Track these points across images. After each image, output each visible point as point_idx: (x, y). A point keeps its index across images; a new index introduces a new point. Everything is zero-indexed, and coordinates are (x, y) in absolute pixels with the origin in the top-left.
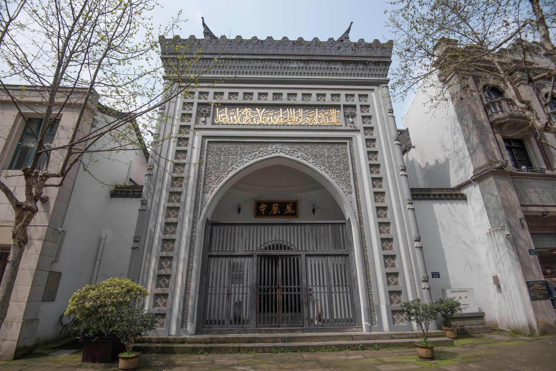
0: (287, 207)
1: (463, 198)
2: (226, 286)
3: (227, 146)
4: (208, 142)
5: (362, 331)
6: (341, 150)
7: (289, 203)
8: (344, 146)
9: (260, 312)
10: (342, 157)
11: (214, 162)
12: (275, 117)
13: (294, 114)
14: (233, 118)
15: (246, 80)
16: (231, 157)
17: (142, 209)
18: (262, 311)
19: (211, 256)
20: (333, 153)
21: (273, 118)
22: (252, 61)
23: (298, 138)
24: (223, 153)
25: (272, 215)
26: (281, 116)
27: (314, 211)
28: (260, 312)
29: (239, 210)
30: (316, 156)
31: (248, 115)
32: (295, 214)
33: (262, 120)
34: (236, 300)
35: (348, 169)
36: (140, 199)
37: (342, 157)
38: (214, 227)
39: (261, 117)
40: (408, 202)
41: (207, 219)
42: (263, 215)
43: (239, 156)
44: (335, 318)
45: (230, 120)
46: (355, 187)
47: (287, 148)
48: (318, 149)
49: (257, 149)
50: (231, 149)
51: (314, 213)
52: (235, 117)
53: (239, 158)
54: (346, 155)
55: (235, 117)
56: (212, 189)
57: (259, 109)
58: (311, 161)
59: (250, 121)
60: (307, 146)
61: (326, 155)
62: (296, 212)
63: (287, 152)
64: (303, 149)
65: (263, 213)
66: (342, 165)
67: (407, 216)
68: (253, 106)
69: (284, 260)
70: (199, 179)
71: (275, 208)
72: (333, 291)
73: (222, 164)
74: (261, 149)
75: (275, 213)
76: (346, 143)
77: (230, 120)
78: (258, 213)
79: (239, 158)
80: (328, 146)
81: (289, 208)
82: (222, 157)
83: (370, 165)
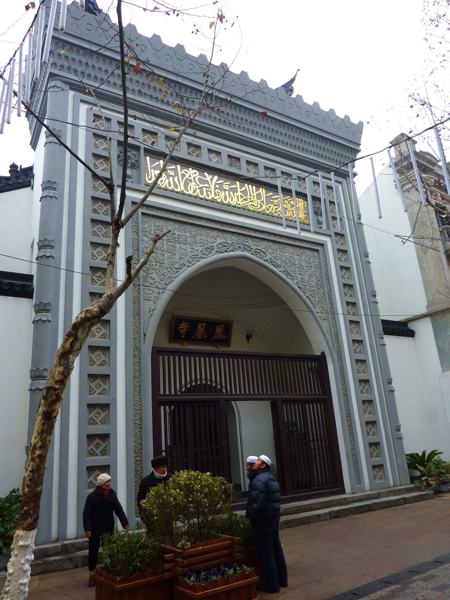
1: (411, 334)
5: (343, 492)
8: (315, 254)
12: (231, 193)
13: (255, 194)
14: (174, 181)
15: (216, 132)
16: (178, 246)
21: (230, 195)
22: (328, 142)
23: (281, 236)
25: (195, 340)
26: (239, 193)
31: (195, 182)
33: (216, 195)
39: (213, 188)
45: (169, 183)
51: (248, 341)
52: (176, 179)
53: (189, 250)
55: (176, 179)
57: (209, 174)
59: (198, 191)
65: (183, 337)
68: (202, 167)
69: (182, 409)
71: (201, 329)
76: (318, 251)
77: (169, 183)
81: (219, 330)
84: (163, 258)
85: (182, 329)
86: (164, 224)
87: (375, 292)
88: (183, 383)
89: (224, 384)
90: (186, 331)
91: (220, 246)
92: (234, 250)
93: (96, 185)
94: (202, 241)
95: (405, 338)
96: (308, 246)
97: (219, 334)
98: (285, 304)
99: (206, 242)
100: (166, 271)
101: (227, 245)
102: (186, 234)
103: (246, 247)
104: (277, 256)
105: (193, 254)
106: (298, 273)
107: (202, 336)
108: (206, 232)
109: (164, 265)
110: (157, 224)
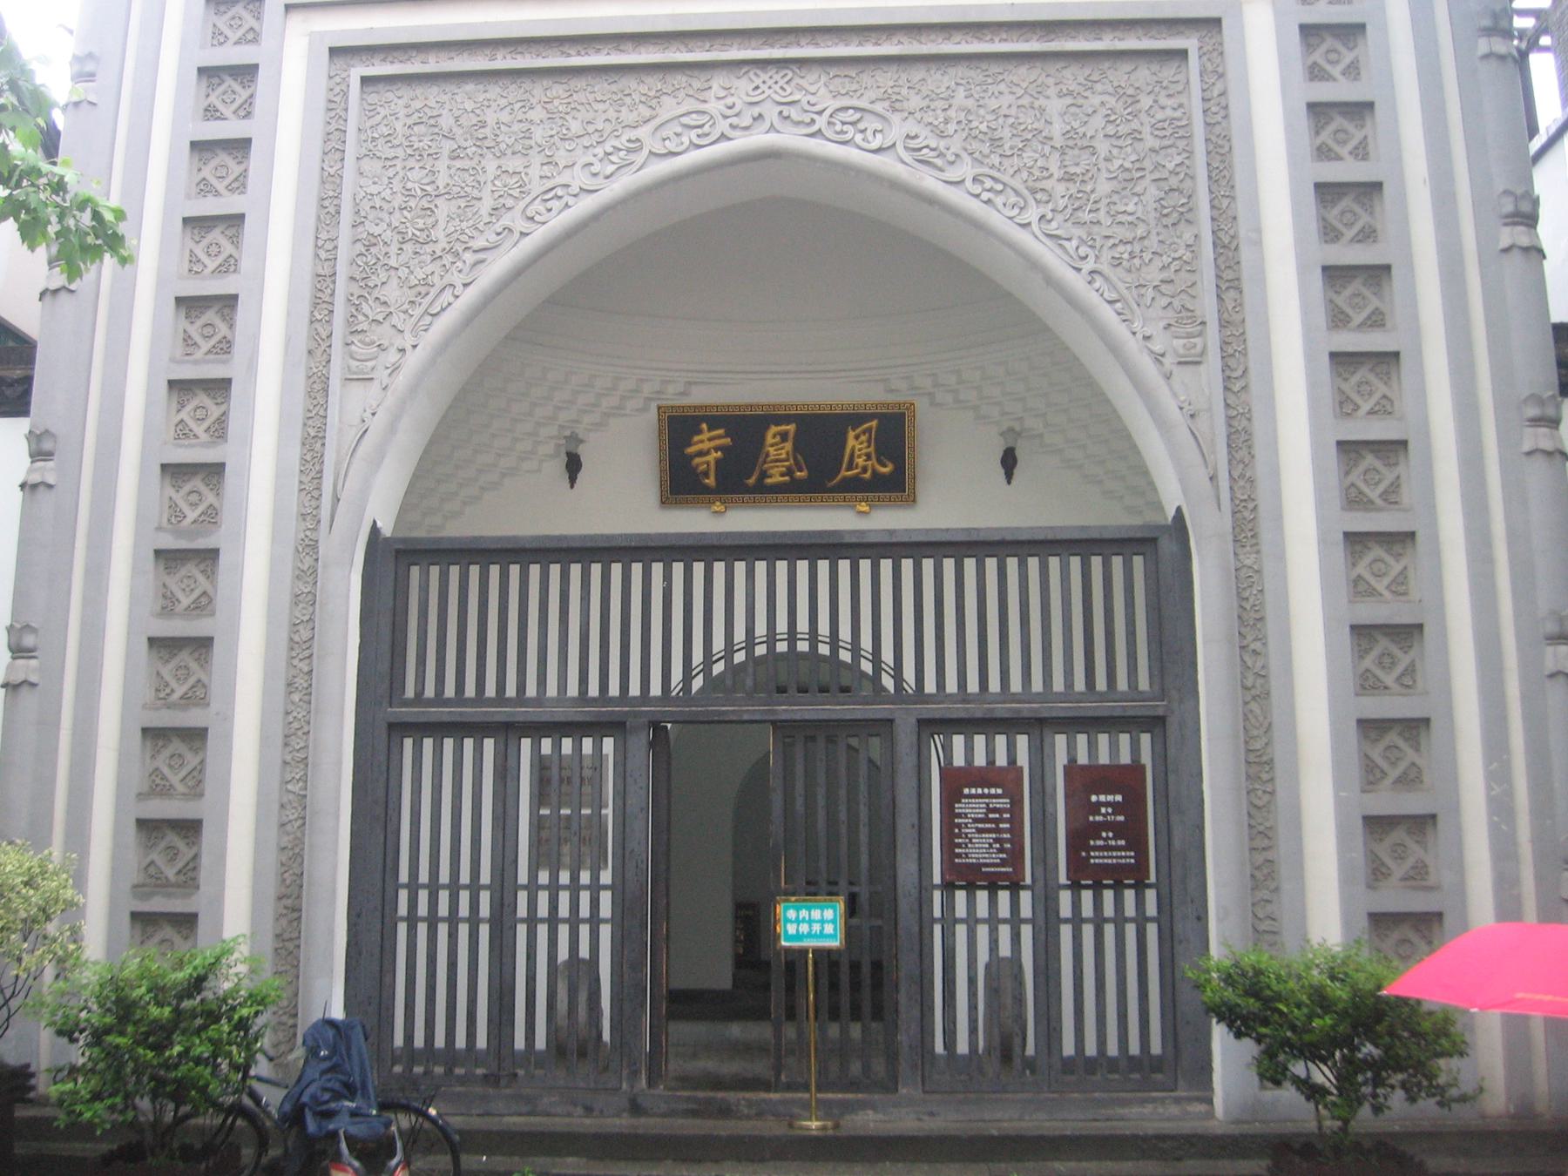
0: (851, 442)
2: (485, 878)
3: (466, 97)
4: (365, 81)
6: (1146, 102)
7: (854, 419)
8: (1168, 72)
9: (877, 966)
10: (1151, 142)
11: (398, 201)
16: (491, 166)
17: (35, 478)
18: (866, 969)
19: (399, 729)
20: (1098, 121)
24: (448, 146)
27: (1009, 462)
28: (877, 966)
29: (574, 466)
30: (996, 142)
32: (894, 481)
34: (563, 954)
35: (1186, 216)
36: (20, 426)
37: (1151, 142)
38: (415, 571)
40: (1533, 411)
41: (375, 530)
42: (707, 490)
43: (536, 159)
44: (1068, 1049)
46: (1224, 324)
47: (819, 91)
48: (1007, 99)
49: (645, 112)
50: (491, 117)
51: (1009, 476)
53: (535, 171)
54: (1178, 131)
56: (392, 357)
58: (966, 170)
60: (940, 80)
61: (1057, 129)
62: (900, 469)
63: (821, 122)
64: (915, 102)
65: (711, 481)
66: (1153, 192)
67: (1515, 494)
70: (321, 300)
71: (778, 451)
72: (1065, 910)
73: (444, 208)
74: (669, 108)
75: (776, 478)
76: (1183, 54)
78: (680, 483)
79: (535, 171)
80: (1073, 76)
81: (856, 444)
82: (442, 165)
83: (1320, 187)
84: (430, 221)
85: (701, 454)
86: (445, 98)
87: (1536, 202)
88: (698, 657)
89: (887, 655)
90: (718, 461)
91: (668, 131)
92: (737, 133)
93: (221, 25)
94: (591, 129)
95: (1375, 812)
96: (1131, 43)
97: (860, 461)
98: (1046, 329)
99: (608, 128)
100: (435, 267)
101: (704, 119)
102: (532, 115)
103: (794, 113)
104: (946, 122)
105: (549, 184)
106: (1057, 174)
107: (789, 472)
108: (614, 88)
109: (428, 248)
110: (418, 104)
